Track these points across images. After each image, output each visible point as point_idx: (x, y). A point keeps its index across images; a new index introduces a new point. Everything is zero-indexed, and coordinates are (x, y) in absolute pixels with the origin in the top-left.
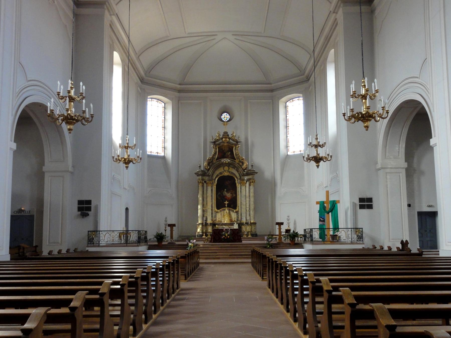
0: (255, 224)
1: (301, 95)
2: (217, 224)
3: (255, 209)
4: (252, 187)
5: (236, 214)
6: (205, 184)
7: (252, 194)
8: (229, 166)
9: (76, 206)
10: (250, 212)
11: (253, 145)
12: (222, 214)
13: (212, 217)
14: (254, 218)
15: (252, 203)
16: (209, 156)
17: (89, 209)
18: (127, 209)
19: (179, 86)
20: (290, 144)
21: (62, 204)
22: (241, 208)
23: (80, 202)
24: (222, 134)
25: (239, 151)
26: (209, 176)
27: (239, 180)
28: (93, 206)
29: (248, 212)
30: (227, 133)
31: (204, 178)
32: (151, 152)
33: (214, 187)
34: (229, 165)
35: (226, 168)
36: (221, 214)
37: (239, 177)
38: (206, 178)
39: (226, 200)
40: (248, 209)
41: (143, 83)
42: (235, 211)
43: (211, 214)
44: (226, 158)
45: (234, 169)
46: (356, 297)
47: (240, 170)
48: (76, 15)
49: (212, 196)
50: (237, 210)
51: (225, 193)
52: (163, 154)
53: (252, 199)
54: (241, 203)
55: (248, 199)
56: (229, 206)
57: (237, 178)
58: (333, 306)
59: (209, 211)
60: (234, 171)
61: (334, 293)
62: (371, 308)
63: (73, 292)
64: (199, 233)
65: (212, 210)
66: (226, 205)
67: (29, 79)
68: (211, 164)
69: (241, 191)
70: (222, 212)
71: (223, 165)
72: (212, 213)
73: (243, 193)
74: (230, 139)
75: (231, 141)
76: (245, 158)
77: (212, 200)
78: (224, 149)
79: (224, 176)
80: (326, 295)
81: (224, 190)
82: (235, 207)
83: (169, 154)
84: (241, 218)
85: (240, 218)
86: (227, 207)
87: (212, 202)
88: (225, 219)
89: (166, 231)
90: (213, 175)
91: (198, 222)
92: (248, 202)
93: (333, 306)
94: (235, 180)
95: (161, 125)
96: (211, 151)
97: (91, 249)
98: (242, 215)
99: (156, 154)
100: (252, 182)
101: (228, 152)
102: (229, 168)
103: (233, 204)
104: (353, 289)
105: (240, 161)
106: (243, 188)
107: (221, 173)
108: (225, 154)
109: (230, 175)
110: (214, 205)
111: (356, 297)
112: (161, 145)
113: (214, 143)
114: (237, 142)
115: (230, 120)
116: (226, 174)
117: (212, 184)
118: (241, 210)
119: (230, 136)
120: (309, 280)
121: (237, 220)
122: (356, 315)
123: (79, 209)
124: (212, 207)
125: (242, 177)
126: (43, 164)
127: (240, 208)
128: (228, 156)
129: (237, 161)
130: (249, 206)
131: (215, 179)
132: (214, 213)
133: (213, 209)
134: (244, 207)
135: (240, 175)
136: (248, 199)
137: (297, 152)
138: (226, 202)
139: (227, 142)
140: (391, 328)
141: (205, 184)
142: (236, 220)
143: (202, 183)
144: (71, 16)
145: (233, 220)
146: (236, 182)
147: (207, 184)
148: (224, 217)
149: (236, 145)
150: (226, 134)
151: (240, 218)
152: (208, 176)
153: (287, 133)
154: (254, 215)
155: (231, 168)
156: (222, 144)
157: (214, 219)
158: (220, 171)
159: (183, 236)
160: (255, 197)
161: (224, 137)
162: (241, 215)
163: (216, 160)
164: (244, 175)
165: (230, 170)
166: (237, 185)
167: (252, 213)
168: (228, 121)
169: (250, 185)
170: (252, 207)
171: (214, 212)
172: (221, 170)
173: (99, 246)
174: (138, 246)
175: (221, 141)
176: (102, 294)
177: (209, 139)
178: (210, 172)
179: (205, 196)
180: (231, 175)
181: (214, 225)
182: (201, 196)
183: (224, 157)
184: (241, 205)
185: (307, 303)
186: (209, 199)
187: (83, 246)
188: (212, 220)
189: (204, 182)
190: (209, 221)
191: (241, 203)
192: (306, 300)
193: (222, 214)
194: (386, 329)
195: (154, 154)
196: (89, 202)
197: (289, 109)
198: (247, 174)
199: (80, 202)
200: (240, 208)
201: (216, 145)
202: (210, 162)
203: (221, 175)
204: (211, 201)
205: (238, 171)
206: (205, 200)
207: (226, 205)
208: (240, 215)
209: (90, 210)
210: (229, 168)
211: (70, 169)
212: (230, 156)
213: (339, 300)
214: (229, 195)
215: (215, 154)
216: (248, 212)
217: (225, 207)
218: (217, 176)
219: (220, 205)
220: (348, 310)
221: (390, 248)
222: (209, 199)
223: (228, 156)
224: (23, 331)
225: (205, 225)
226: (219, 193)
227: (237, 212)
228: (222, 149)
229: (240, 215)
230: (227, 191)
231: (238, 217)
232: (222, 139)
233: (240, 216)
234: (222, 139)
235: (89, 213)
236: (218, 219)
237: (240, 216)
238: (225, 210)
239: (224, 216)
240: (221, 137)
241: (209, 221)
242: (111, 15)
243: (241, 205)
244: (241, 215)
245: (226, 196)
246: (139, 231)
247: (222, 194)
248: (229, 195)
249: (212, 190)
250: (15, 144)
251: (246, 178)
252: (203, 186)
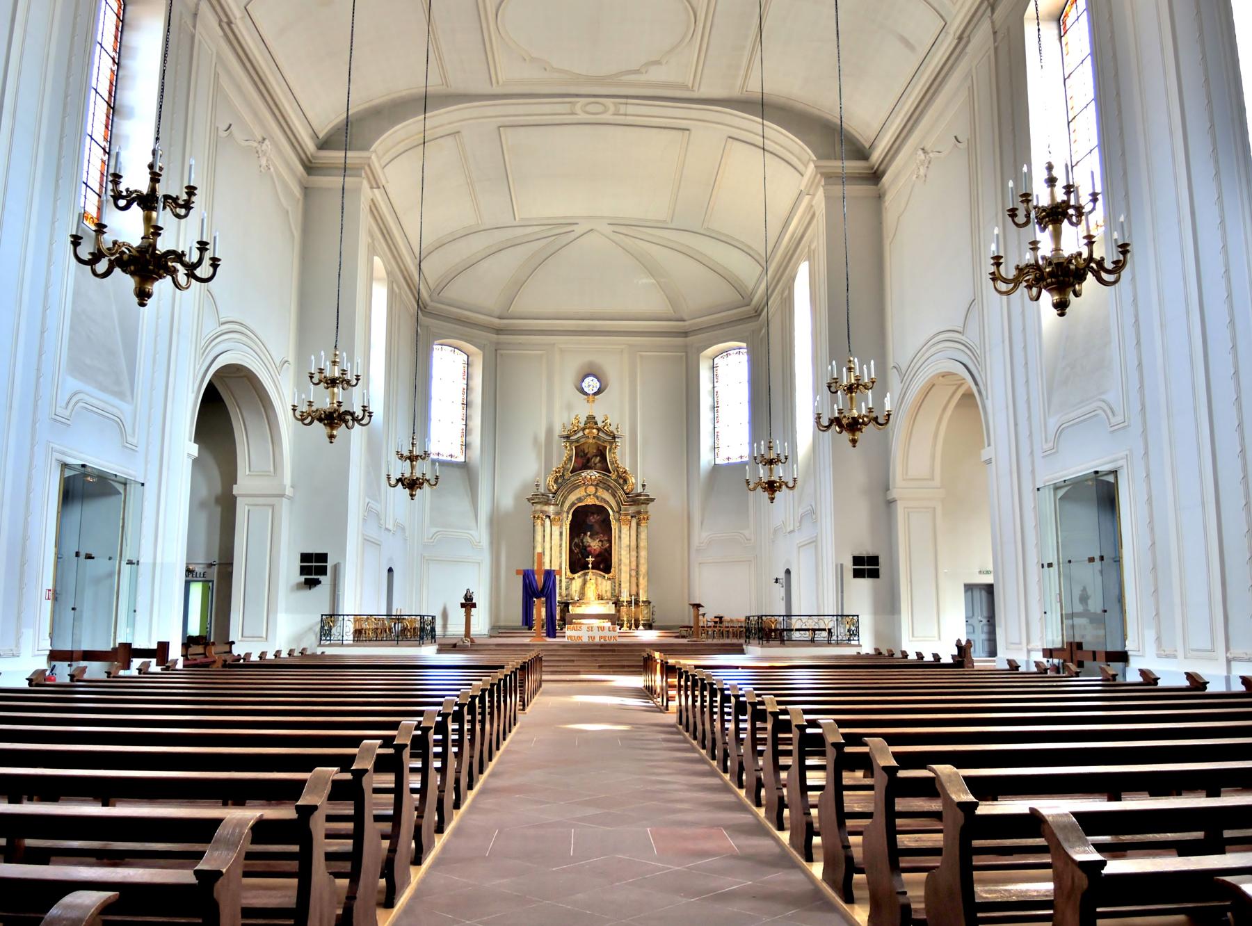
1: (744, 345)
9: (297, 564)
16: (557, 464)
17: (323, 571)
18: (390, 570)
19: (497, 321)
20: (722, 442)
22: (620, 570)
23: (305, 557)
24: (583, 420)
28: (329, 565)
29: (634, 580)
37: (616, 509)
41: (427, 317)
44: (590, 468)
46: (896, 755)
47: (620, 493)
48: (306, 190)
52: (462, 459)
55: (634, 553)
56: (596, 566)
58: (845, 774)
60: (607, 496)
61: (848, 749)
62: (932, 775)
63: (355, 742)
67: (222, 320)
73: (625, 540)
74: (599, 430)
80: (831, 753)
90: (563, 502)
93: (845, 774)
95: (459, 398)
96: (563, 455)
97: (329, 651)
103: (604, 563)
104: (892, 740)
106: (625, 529)
107: (580, 500)
108: (589, 460)
109: (598, 503)
111: (896, 755)
112: (458, 440)
113: (568, 437)
115: (599, 392)
116: (590, 501)
119: (600, 425)
120: (794, 723)
122: (897, 788)
123: (304, 571)
126: (234, 480)
129: (614, 476)
134: (625, 569)
137: (735, 459)
138: (590, 559)
140: (968, 808)
144: (297, 191)
149: (611, 443)
150: (591, 419)
153: (715, 420)
155: (600, 490)
156: (583, 440)
159: (500, 628)
168: (595, 394)
169: (638, 524)
172: (580, 493)
173: (342, 645)
174: (420, 645)
175: (581, 434)
176: (400, 748)
177: (558, 430)
185: (786, 768)
187: (312, 645)
191: (620, 560)
192: (783, 761)
194: (958, 810)
196: (323, 557)
197: (720, 371)
199: (305, 557)
201: (571, 443)
205: (614, 496)
209: (325, 574)
211: (289, 491)
213: (864, 762)
214: (595, 544)
218: (573, 504)
220: (880, 780)
221: (920, 656)
224: (298, 808)
232: (584, 429)
234: (584, 429)
235: (322, 578)
240: (582, 425)
242: (372, 188)
246: (422, 617)
250: (196, 446)
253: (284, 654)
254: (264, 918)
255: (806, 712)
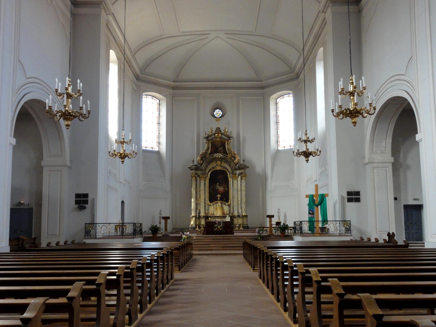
0: (246, 216)
1: (291, 92)
2: (210, 217)
3: (246, 202)
4: (243, 181)
5: (228, 207)
6: (198, 178)
7: (243, 188)
8: (221, 161)
9: (73, 199)
10: (241, 205)
11: (244, 140)
12: (215, 207)
13: (205, 210)
14: (246, 211)
15: (244, 196)
16: (202, 151)
17: (86, 202)
18: (123, 202)
19: (173, 83)
20: (281, 140)
21: (60, 197)
22: (233, 201)
23: (77, 196)
24: (214, 130)
25: (231, 146)
26: (202, 170)
27: (231, 175)
28: (90, 199)
29: (240, 206)
30: (220, 129)
31: (198, 172)
32: (146, 147)
33: (207, 181)
34: (221, 159)
35: (219, 163)
36: (214, 207)
37: (231, 172)
38: (199, 172)
39: (218, 193)
40: (239, 202)
41: (139, 81)
42: (227, 204)
43: (204, 207)
44: (218, 152)
45: (227, 163)
46: (344, 288)
47: (232, 164)
48: (73, 15)
49: (205, 189)
50: (229, 203)
51: (218, 186)
52: (157, 149)
53: (244, 193)
54: (233, 196)
55: (239, 193)
56: (221, 199)
57: (229, 172)
58: (322, 296)
59: (202, 204)
60: (227, 166)
61: (323, 284)
62: (359, 298)
63: (71, 283)
64: (192, 225)
65: (205, 203)
66: (219, 199)
67: (28, 77)
68: (204, 159)
69: (233, 185)
70: (215, 205)
71: (216, 159)
72: (205, 206)
73: (235, 187)
74: (222, 134)
75: (223, 136)
76: (237, 153)
77: (205, 193)
78: (216, 144)
79: (216, 170)
80: (315, 285)
81: (216, 184)
82: (227, 200)
83: (163, 149)
84: (233, 211)
85: (232, 211)
86: (220, 200)
87: (205, 195)
88: (217, 212)
89: (160, 223)
90: (206, 169)
91: (191, 215)
92: (239, 195)
93: (322, 296)
94: (227, 174)
95: (156, 121)
96: (204, 146)
97: (88, 241)
98: (234, 208)
99: (151, 149)
100: (244, 176)
101: (221, 147)
102: (221, 163)
103: (225, 198)
104: (341, 279)
105: (232, 156)
106: (235, 182)
107: (213, 168)
108: (217, 149)
109: (222, 169)
110: (207, 199)
111: (344, 288)
112: (155, 140)
113: (207, 138)
114: (229, 137)
115: (222, 116)
116: (219, 168)
117: (205, 178)
118: (233, 203)
119: (222, 132)
120: (299, 271)
121: (230, 213)
122: (344, 304)
123: (77, 202)
124: (205, 200)
125: (234, 172)
126: (42, 159)
127: (232, 201)
128: (221, 151)
129: (229, 156)
130: (241, 199)
131: (208, 174)
132: (207, 206)
133: (206, 202)
134: (236, 200)
135: (232, 170)
136: (239, 193)
137: (287, 147)
138: (219, 196)
139: (220, 138)
140: (378, 317)
141: (198, 178)
142: (228, 212)
143: (196, 177)
144: (69, 15)
145: (226, 213)
146: (229, 176)
147: (200, 178)
148: (217, 210)
149: (228, 140)
150: (218, 129)
151: (232, 211)
152: (201, 170)
153: (277, 129)
154: (246, 208)
155: (223, 163)
156: (214, 139)
157: (207, 212)
158: (213, 166)
159: (177, 229)
160: (246, 190)
161: (216, 132)
162: (233, 208)
163: (209, 155)
164: (236, 169)
165: (222, 165)
166: (229, 179)
167: (243, 206)
168: (221, 117)
169: (241, 179)
170: (244, 200)
171: (206, 205)
172: (213, 164)
173: (96, 238)
174: (133, 238)
175: (214, 136)
176: (99, 285)
177: (202, 135)
178: (203, 167)
179: (198, 190)
180: (224, 169)
181: (206, 217)
182: (194, 190)
183: (216, 152)
184: (233, 198)
185: (296, 293)
186: (202, 193)
187: (80, 238)
188: (205, 213)
189: (197, 176)
190: (202, 214)
191: (233, 196)
192: (296, 290)
193: (215, 207)
194: (373, 318)
195: (149, 149)
196: (86, 196)
197: (280, 105)
198: (239, 169)
199: (77, 196)
200: (232, 201)
201: (209, 141)
202: (203, 157)
203: (214, 170)
204: (204, 194)
205: (230, 166)
206: (198, 193)
207: (219, 199)
208: (232, 208)
209: (87, 204)
210: (221, 163)
211: (68, 164)
212: (222, 151)
213: (328, 290)
214: (221, 189)
215: (208, 149)
216: (240, 206)
217: (218, 200)
218: (210, 170)
219: (212, 199)
220: (336, 300)
221: (377, 240)
222: (202, 193)
223: (221, 151)
224: (22, 320)
225: (198, 217)
226: (212, 187)
227: (229, 205)
228: (215, 144)
229: (232, 208)
230: (219, 185)
231: (230, 210)
232: (215, 134)
233: (232, 209)
234: (215, 134)
235: (86, 206)
236: (210, 212)
237: (232, 209)
238: (217, 203)
239: (216, 209)
240: (214, 132)
241: (202, 214)
242: (107, 14)
243: (233, 198)
244: (233, 208)
245: (218, 190)
246: (134, 224)
247: (215, 188)
248: (221, 189)
249: (205, 184)
250: (15, 140)
251: (238, 172)
252: (196, 180)
253: (62, 243)
254: (424, 293)
255: (305, 266)
